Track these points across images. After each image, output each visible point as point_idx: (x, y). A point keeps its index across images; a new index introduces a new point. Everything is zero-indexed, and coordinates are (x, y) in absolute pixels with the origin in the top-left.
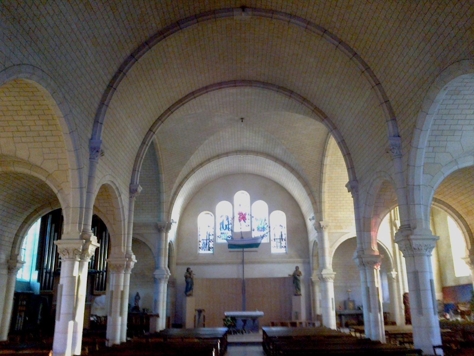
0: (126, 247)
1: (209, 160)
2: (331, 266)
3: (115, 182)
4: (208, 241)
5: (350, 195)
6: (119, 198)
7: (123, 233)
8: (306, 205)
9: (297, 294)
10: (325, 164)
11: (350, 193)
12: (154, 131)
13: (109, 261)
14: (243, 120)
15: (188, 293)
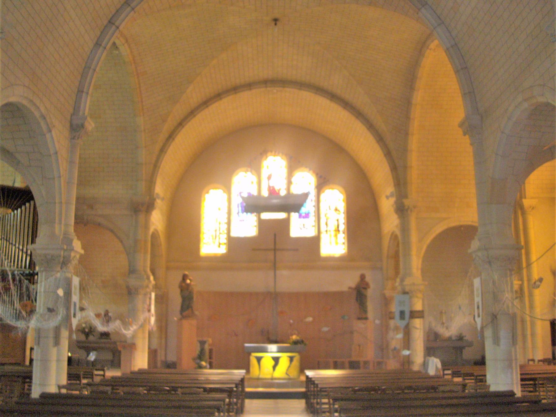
1: (218, 96)
2: (419, 272)
3: (38, 102)
4: (218, 232)
5: (467, 140)
6: (48, 136)
9: (362, 317)
11: (467, 136)
12: (117, 23)
13: (34, 249)
14: (278, 23)
15: (184, 314)
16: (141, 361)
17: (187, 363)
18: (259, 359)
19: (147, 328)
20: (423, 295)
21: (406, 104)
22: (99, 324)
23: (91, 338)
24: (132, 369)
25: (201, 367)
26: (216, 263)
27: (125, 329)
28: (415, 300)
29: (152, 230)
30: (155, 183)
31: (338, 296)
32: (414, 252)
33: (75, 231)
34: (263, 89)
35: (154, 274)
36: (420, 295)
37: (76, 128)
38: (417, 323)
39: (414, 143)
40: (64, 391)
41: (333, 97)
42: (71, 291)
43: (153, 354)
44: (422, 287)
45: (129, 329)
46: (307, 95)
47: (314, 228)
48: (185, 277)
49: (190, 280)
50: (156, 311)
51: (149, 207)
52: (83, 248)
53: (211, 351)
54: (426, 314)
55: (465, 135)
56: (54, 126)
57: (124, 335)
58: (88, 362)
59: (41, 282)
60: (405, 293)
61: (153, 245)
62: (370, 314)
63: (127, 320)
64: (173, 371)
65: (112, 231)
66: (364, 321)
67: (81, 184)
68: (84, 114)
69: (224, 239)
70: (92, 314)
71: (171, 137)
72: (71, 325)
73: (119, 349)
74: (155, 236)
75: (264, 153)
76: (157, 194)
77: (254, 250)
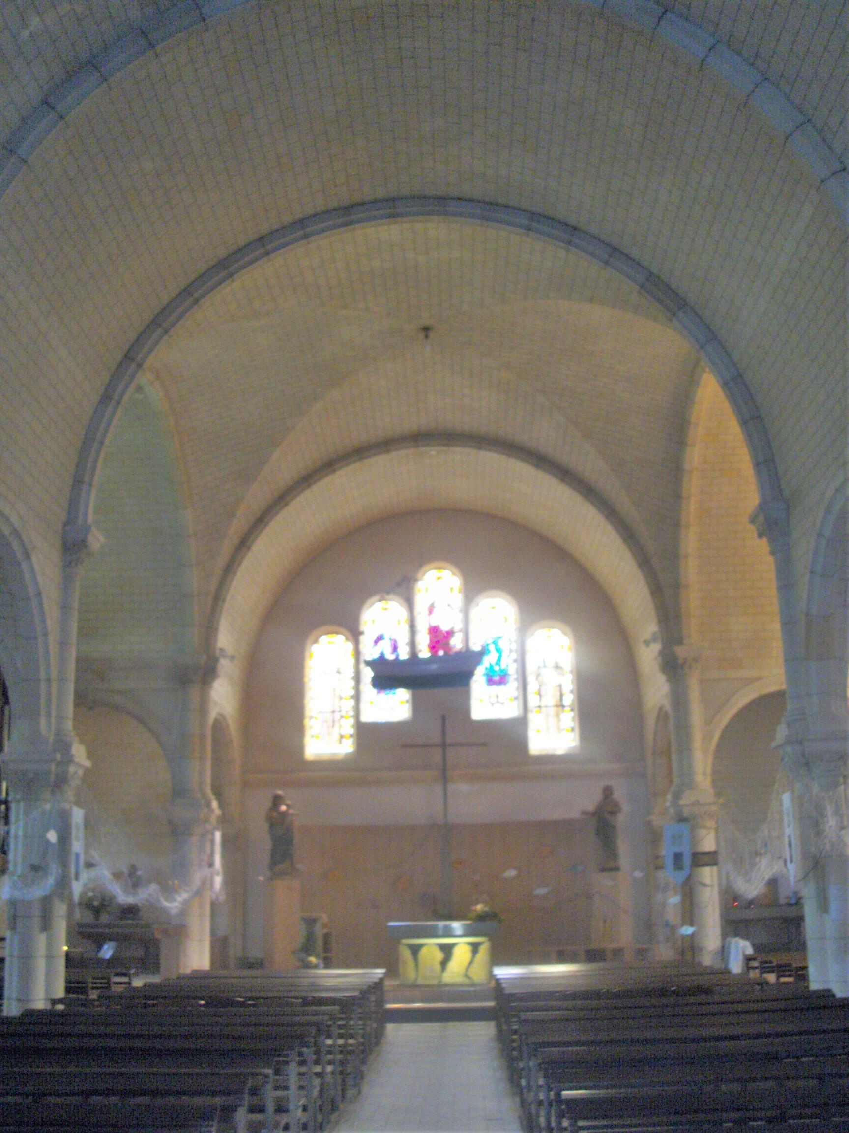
0: (53, 720)
1: (329, 466)
2: (709, 779)
5: (763, 546)
6: (25, 566)
7: (43, 675)
8: (644, 623)
9: (609, 866)
10: (687, 466)
11: (764, 540)
12: (139, 358)
14: (431, 335)
16: (197, 957)
17: (283, 956)
18: (415, 950)
19: (208, 896)
20: (717, 823)
21: (674, 469)
22: (119, 891)
23: (105, 918)
24: (182, 971)
25: (308, 966)
26: (332, 773)
27: (167, 900)
28: (702, 832)
29: (213, 715)
30: (217, 630)
31: (560, 829)
32: (697, 744)
33: (75, 728)
34: (411, 451)
35: (218, 794)
36: (711, 823)
37: (73, 547)
38: (708, 874)
39: (690, 540)
40: (60, 1007)
41: (540, 460)
42: (70, 834)
43: (220, 946)
44: (714, 808)
45: (174, 900)
46: (492, 459)
47: (515, 703)
48: (277, 801)
49: (287, 805)
50: (225, 865)
51: (208, 673)
52: (90, 755)
53: (327, 938)
54: (721, 858)
55: (760, 536)
56: (35, 547)
57: (165, 911)
58: (100, 961)
59: (17, 820)
60: (682, 820)
61: (216, 743)
62: (624, 861)
63: (170, 883)
64: (255, 972)
65: (140, 720)
66: (613, 874)
67: (85, 633)
68: (86, 521)
69: (348, 726)
70: (107, 873)
71: (244, 543)
72: (71, 893)
73: (158, 935)
74: (219, 726)
75: (423, 558)
76: (222, 650)
77: (405, 746)
